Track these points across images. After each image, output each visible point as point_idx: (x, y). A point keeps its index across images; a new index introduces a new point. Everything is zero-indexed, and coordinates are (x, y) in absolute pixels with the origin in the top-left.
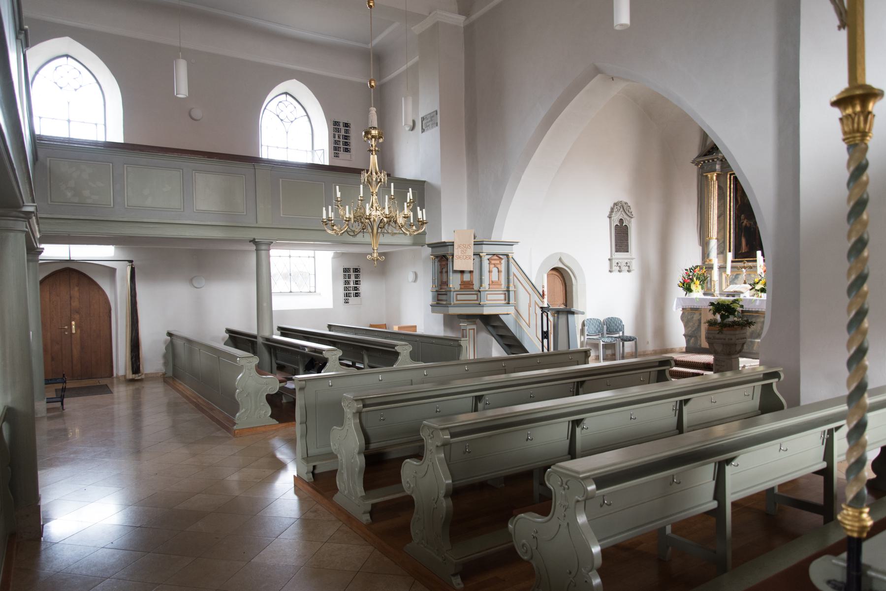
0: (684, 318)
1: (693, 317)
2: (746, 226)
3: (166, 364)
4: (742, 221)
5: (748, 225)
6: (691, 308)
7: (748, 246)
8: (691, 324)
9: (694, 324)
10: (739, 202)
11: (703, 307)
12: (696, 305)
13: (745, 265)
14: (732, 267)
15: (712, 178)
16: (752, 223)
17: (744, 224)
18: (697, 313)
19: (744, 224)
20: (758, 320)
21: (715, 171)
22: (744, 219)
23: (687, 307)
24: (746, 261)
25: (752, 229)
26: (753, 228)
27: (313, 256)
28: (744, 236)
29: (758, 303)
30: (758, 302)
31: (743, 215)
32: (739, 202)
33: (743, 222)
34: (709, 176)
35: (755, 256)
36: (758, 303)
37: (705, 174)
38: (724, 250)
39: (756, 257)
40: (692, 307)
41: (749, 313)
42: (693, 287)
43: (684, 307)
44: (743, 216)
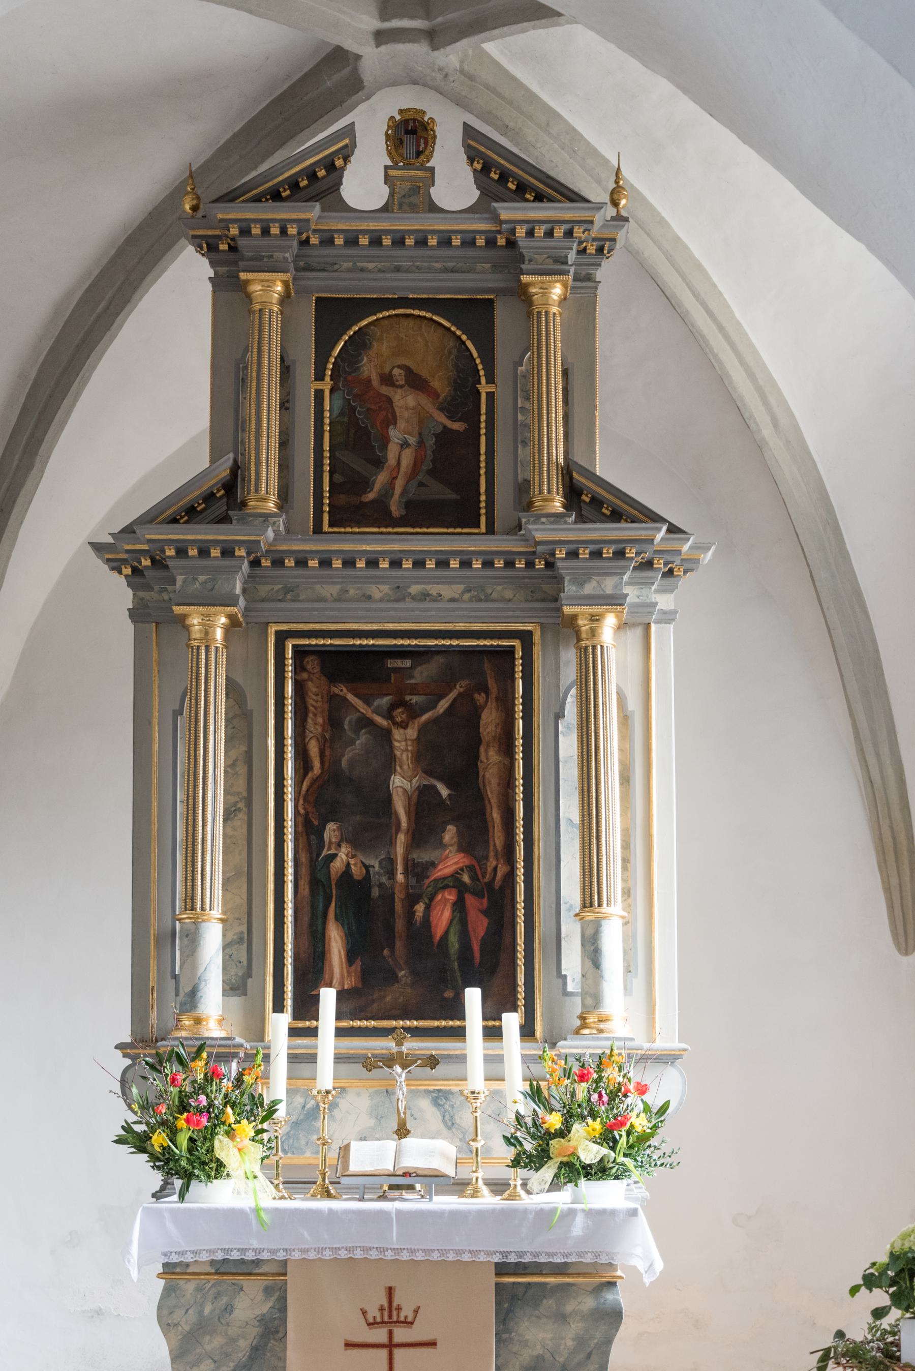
0: (178, 1314)
1: (229, 1309)
2: (347, 872)
3: (216, 454)
4: (325, 852)
5: (357, 871)
6: (213, 1262)
7: (358, 964)
8: (212, 1343)
9: (233, 1341)
10: (317, 764)
11: (296, 1255)
12: (255, 1244)
13: (404, 1049)
14: (340, 1059)
15: (207, 633)
16: (375, 863)
17: (337, 865)
18: (253, 1287)
19: (337, 865)
20: (569, 1308)
21: (228, 601)
22: (339, 845)
23: (265, 1256)
24: (407, 1029)
25: (375, 892)
26: (381, 885)
27: (252, 1298)
28: (336, 919)
29: (578, 1227)
30: (580, 1220)
31: (331, 826)
32: (317, 764)
33: (335, 856)
34: (195, 621)
35: (457, 1010)
36: (578, 1227)
37: (178, 610)
38: (248, 974)
39: (463, 1018)
40: (220, 1256)
41: (541, 1274)
42: (224, 1148)
43: (174, 1259)
44: (331, 831)
